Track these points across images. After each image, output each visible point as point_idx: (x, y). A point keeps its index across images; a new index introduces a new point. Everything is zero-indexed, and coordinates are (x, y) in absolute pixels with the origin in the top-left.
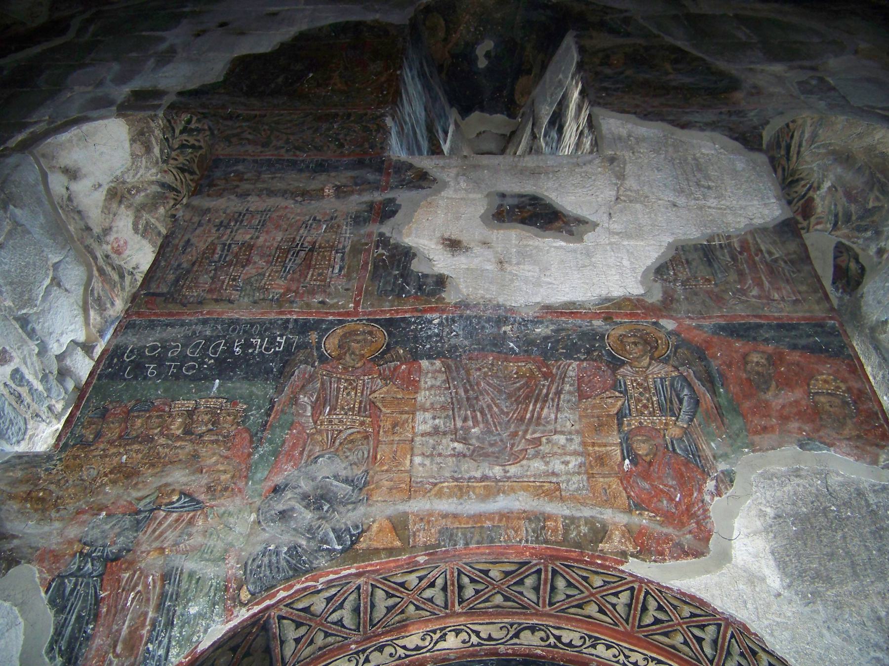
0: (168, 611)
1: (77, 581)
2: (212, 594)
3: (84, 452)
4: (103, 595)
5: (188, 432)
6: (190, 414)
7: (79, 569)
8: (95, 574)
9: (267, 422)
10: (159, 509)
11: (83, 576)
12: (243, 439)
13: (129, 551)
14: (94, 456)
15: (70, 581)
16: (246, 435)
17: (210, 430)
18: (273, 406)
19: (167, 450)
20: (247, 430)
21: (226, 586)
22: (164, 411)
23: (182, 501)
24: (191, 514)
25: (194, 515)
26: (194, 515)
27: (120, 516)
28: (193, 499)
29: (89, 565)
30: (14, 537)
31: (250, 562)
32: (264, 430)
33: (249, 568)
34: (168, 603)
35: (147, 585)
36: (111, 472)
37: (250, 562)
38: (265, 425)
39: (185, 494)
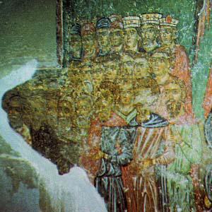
0: (166, 209)
1: (108, 179)
2: (188, 200)
3: (79, 68)
4: (126, 190)
5: (141, 50)
6: (139, 30)
7: (107, 171)
8: (117, 175)
9: (196, 38)
10: (140, 126)
11: (110, 175)
12: (182, 57)
13: (131, 160)
14: (86, 72)
15: (105, 180)
16: (183, 53)
17: (157, 48)
18: (198, 22)
19: (131, 67)
20: (183, 48)
21: (195, 195)
22: (119, 27)
23: (153, 119)
24: (162, 130)
25: (164, 131)
26: (164, 131)
27: (118, 128)
28: (160, 118)
29: (112, 168)
30: (20, 156)
31: (206, 178)
32: (195, 49)
33: (207, 183)
34: (164, 204)
35: (149, 189)
36: (101, 87)
37: (206, 178)
38: (195, 43)
39: (155, 115)
